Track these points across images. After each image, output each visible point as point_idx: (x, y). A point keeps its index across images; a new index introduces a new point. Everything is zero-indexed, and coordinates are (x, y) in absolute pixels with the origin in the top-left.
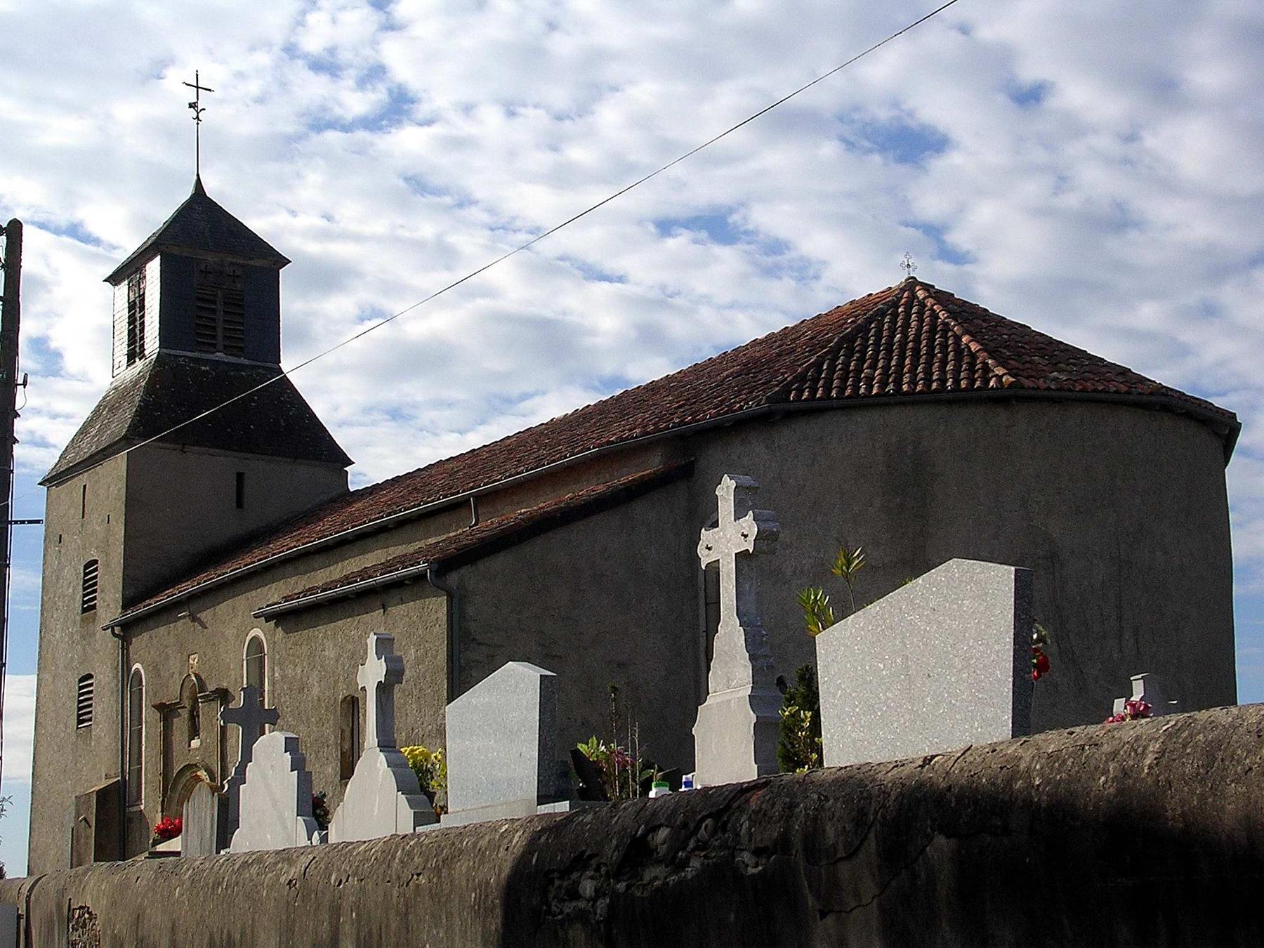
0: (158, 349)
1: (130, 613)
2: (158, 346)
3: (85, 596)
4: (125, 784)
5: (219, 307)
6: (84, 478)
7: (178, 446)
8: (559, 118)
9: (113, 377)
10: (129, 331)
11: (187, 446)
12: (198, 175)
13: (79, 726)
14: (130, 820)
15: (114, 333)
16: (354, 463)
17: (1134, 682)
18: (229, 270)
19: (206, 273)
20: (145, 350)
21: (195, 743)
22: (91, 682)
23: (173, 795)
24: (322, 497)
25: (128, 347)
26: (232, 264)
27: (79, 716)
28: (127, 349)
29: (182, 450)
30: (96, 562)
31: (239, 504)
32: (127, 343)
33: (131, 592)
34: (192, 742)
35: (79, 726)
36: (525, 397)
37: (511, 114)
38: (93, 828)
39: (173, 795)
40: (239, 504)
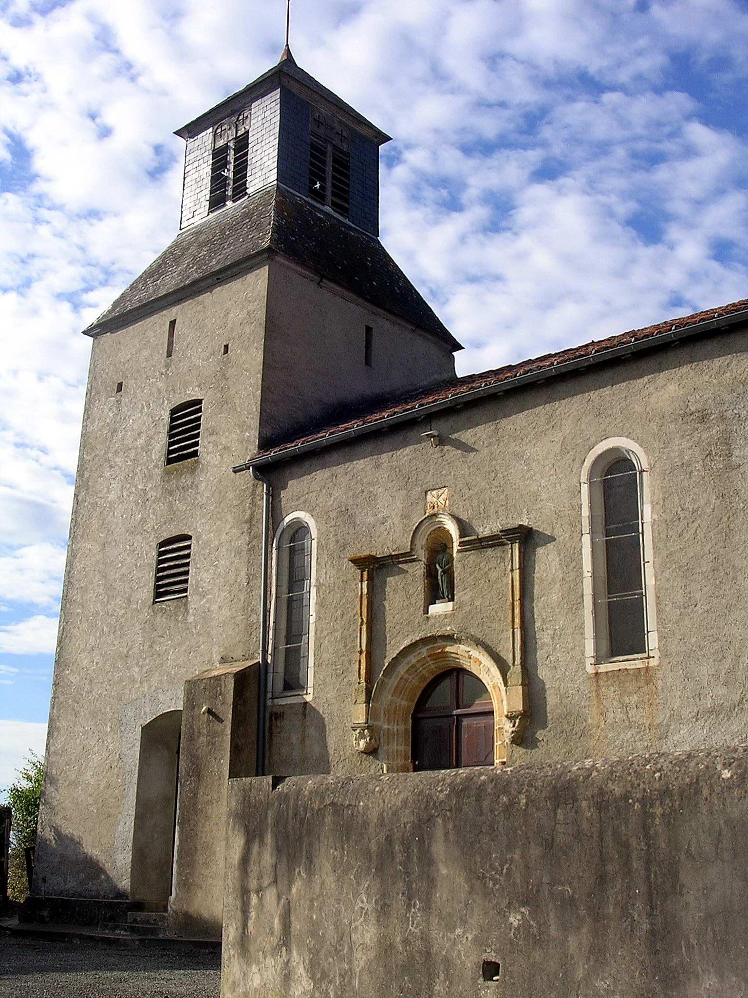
0: (275, 182)
1: (272, 454)
2: (276, 178)
3: (171, 444)
4: (266, 672)
5: (329, 160)
6: (174, 312)
7: (316, 277)
8: (68, 384)
9: (181, 229)
10: (211, 177)
11: (324, 281)
12: (287, 45)
13: (156, 600)
14: (277, 716)
15: (184, 185)
16: (464, 348)
17: (465, 722)
18: (338, 128)
19: (318, 123)
20: (247, 188)
21: (439, 609)
22: (189, 543)
23: (386, 680)
24: (436, 376)
25: (211, 194)
26: (340, 122)
27: (157, 587)
28: (209, 195)
29: (318, 284)
30: (200, 402)
31: (368, 362)
32: (209, 189)
33: (268, 432)
34: (431, 607)
35: (156, 600)
36: (21, 546)
37: (40, 379)
38: (228, 724)
39: (386, 680)
40: (368, 362)
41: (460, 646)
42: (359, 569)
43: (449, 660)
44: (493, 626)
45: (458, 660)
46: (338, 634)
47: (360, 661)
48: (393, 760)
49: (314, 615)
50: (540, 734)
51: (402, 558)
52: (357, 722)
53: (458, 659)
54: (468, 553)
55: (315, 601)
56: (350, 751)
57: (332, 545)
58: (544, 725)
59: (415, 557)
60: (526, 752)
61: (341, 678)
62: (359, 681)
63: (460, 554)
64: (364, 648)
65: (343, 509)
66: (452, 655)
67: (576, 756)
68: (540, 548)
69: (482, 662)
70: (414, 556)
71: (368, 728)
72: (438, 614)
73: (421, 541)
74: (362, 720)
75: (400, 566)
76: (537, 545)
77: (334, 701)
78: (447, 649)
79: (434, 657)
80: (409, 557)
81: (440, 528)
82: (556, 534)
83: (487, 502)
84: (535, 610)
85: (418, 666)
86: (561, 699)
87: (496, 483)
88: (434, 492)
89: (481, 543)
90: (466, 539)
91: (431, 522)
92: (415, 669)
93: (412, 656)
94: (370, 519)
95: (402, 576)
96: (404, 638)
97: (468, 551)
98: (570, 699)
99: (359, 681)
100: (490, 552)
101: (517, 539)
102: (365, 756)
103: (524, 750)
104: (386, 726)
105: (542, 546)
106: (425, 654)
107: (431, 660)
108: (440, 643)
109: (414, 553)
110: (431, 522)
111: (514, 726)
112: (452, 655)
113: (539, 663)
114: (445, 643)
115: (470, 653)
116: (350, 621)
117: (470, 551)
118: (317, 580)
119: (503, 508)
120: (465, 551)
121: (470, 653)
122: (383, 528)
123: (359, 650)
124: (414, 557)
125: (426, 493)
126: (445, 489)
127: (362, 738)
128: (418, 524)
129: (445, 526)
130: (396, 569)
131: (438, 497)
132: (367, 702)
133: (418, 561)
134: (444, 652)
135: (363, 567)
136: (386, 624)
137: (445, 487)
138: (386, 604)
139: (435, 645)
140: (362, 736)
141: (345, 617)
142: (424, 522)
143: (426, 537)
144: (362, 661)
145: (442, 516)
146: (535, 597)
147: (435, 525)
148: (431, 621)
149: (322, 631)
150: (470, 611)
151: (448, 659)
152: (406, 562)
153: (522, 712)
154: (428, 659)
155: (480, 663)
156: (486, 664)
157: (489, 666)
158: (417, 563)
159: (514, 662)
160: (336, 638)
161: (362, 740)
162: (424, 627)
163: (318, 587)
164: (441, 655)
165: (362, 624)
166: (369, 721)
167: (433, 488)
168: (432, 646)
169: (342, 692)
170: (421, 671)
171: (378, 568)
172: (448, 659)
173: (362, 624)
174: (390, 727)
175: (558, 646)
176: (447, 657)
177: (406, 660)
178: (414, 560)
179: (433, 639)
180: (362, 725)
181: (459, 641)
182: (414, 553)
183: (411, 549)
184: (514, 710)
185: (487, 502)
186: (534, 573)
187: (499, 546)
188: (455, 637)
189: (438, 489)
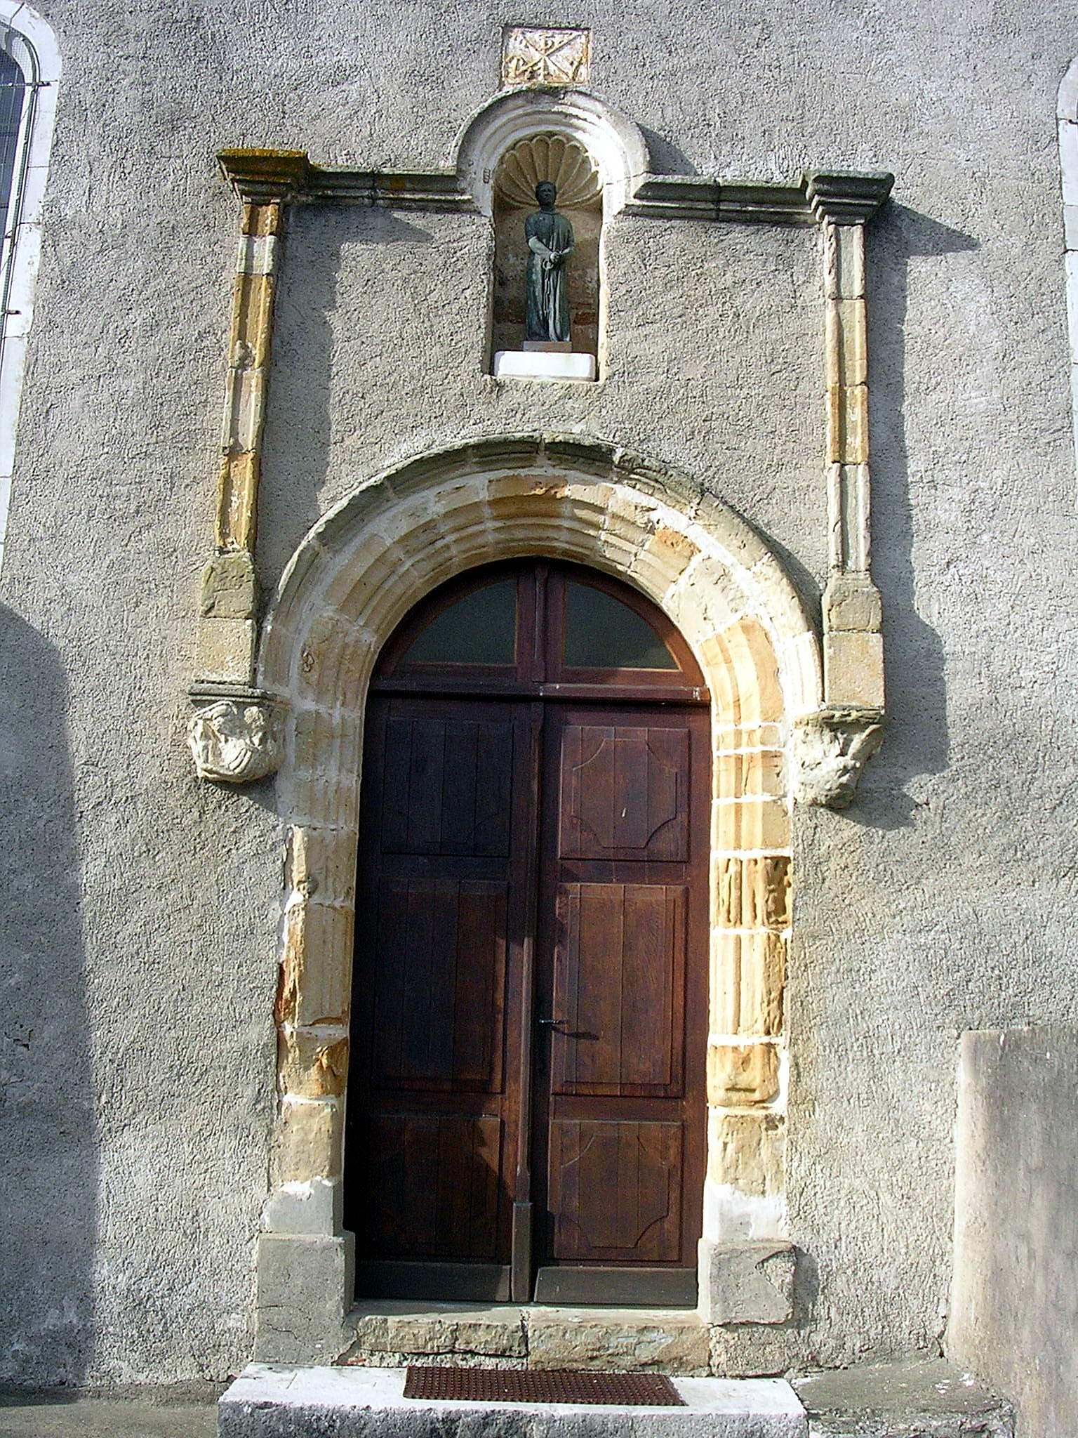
23: (326, 556)
39: (326, 556)
41: (617, 487)
42: (243, 193)
43: (558, 527)
44: (748, 446)
45: (592, 532)
46: (131, 385)
47: (227, 482)
48: (326, 819)
49: (27, 312)
50: (919, 787)
51: (413, 191)
52: (214, 677)
53: (597, 527)
54: (660, 223)
55: (34, 270)
56: (155, 773)
57: (125, 107)
58: (936, 759)
59: (465, 197)
60: (867, 834)
61: (131, 527)
62: (219, 543)
63: (630, 223)
64: (248, 438)
65: (183, 14)
66: (579, 513)
67: (1040, 861)
68: (919, 259)
69: (699, 544)
70: (463, 192)
71: (263, 701)
72: (536, 381)
73: (486, 160)
74: (235, 671)
75: (398, 215)
76: (907, 250)
77: (89, 598)
78: (567, 491)
79: (513, 509)
80: (441, 192)
81: (551, 134)
82: (974, 229)
83: (734, 99)
84: (907, 425)
85: (443, 529)
86: (993, 689)
87: (763, 55)
88: (537, 36)
89: (720, 201)
90: (660, 178)
91: (529, 109)
92: (432, 537)
93: (430, 494)
94: (283, 61)
95: (402, 247)
96: (401, 433)
97: (661, 217)
98: (1023, 693)
99: (219, 543)
100: (739, 235)
101: (860, 215)
102: (219, 794)
103: (859, 829)
104: (309, 705)
105: (927, 254)
106: (484, 496)
107: (495, 518)
108: (544, 469)
109: (463, 185)
110: (529, 109)
111: (843, 754)
112: (579, 513)
113: (920, 578)
114: (558, 472)
115: (654, 516)
116: (181, 349)
117: (670, 219)
118: (50, 206)
119: (790, 125)
120: (652, 217)
121: (654, 516)
122: (331, 96)
123: (225, 441)
124: (458, 198)
125: (507, 28)
126: (575, 33)
127: (232, 733)
128: (490, 106)
129: (578, 135)
130: (379, 222)
131: (550, 51)
132: (258, 615)
133: (467, 212)
134: (554, 497)
135: (264, 189)
136: (329, 378)
137: (576, 29)
138: (336, 320)
139: (523, 472)
140: (235, 726)
141: (162, 335)
142: (511, 104)
143: (501, 150)
144: (236, 482)
145: (581, 101)
146: (909, 388)
147: (540, 123)
148: (511, 399)
149: (58, 368)
150: (663, 392)
151: (557, 522)
152: (423, 207)
153: (883, 712)
154: (487, 512)
155: (693, 550)
156: (715, 557)
157: (727, 563)
158: (466, 218)
159: (844, 562)
160: (118, 400)
161: (233, 741)
162: (480, 410)
163: (53, 231)
164: (544, 507)
165: (243, 363)
166: (260, 678)
167: (536, 22)
168: (511, 473)
169: (131, 575)
170: (447, 547)
171: (306, 207)
172: (557, 522)
173: (243, 363)
174: (322, 709)
175: (985, 537)
176: (558, 516)
177: (414, 500)
178: (455, 208)
179: (527, 450)
180: (239, 690)
181: (629, 470)
182: (463, 185)
183: (459, 170)
184: (854, 704)
185: (734, 99)
186: (902, 321)
187: (776, 224)
188: (616, 458)
189: (548, 28)
